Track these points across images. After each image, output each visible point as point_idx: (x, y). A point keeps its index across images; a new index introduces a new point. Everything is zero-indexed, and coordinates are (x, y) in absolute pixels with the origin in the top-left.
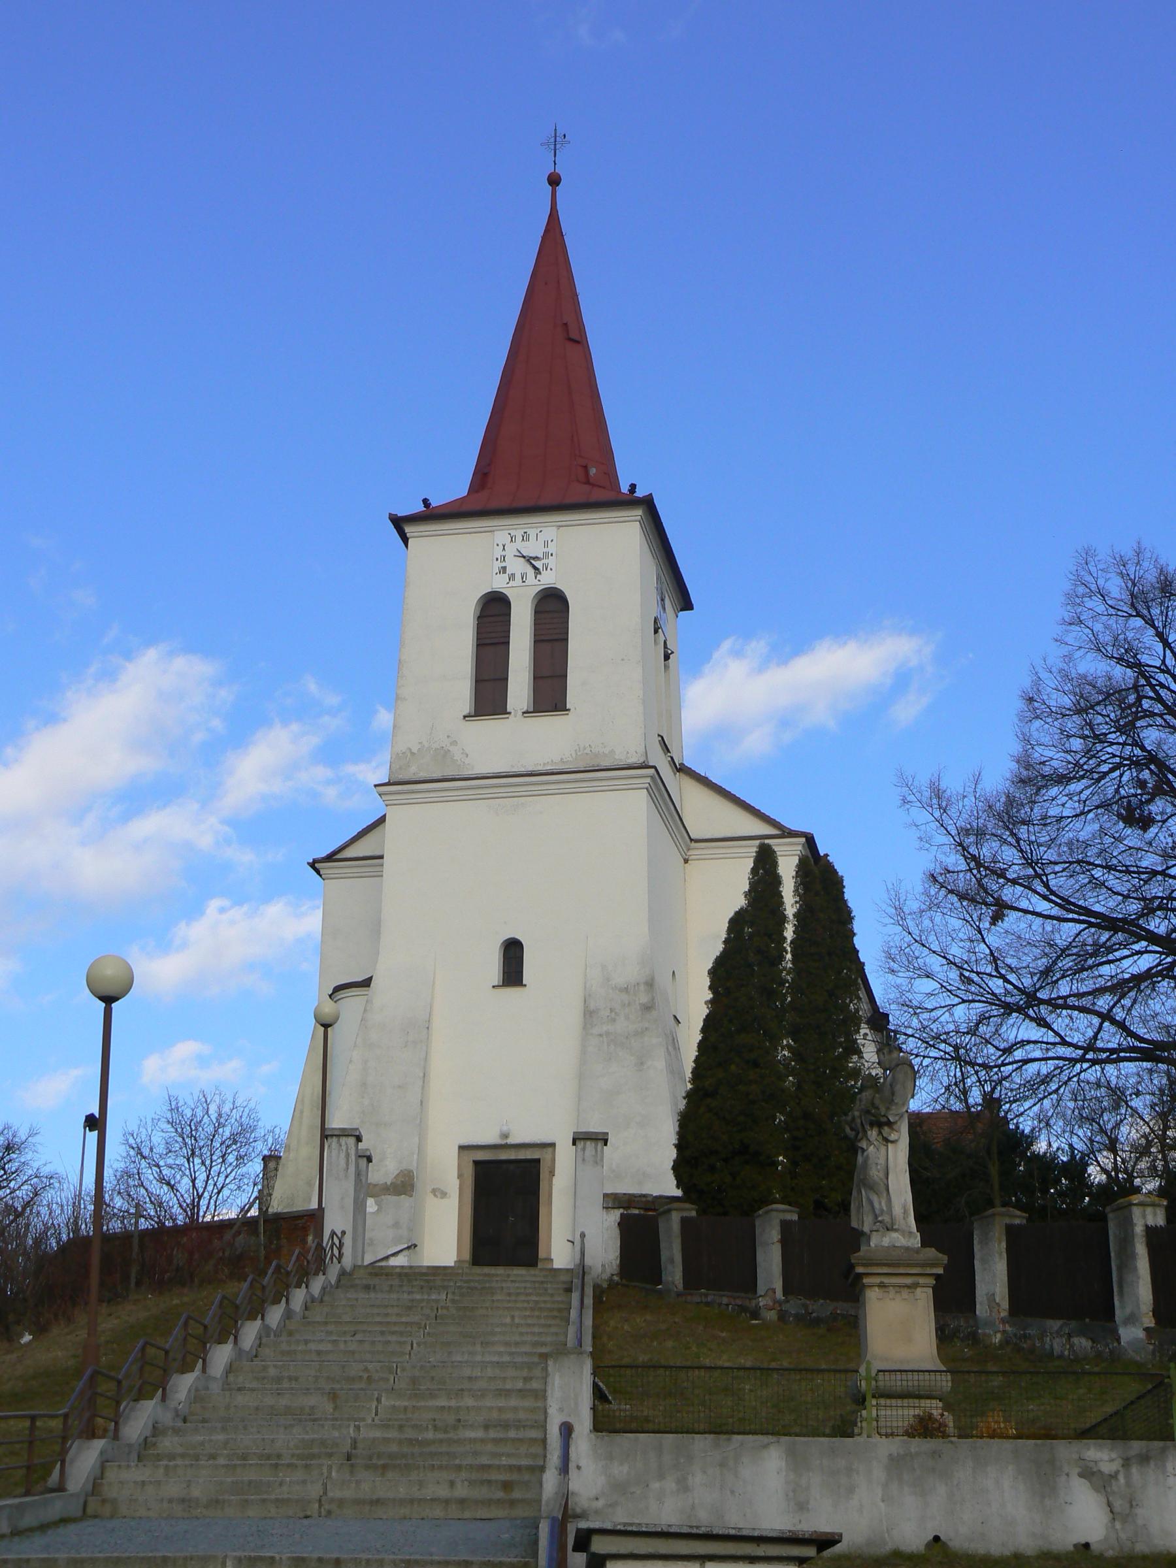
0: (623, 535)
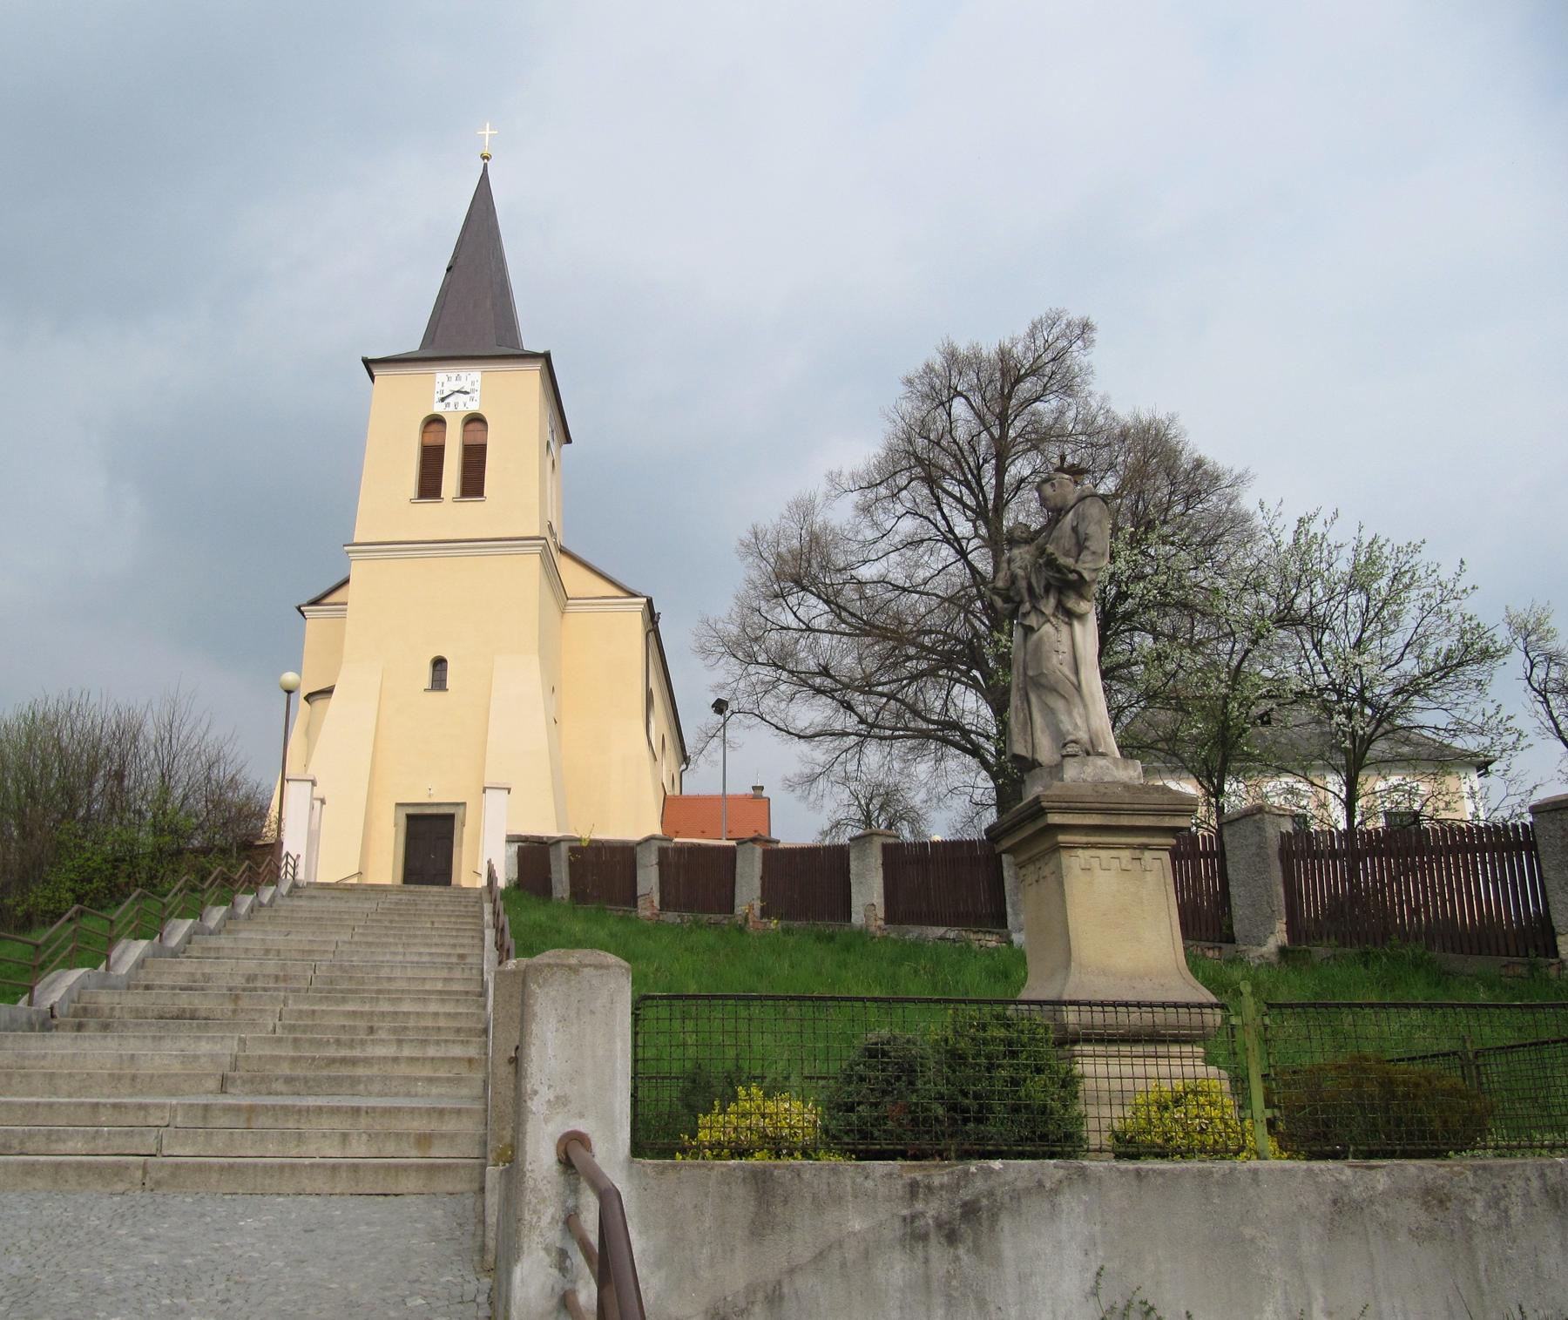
0: (529, 377)
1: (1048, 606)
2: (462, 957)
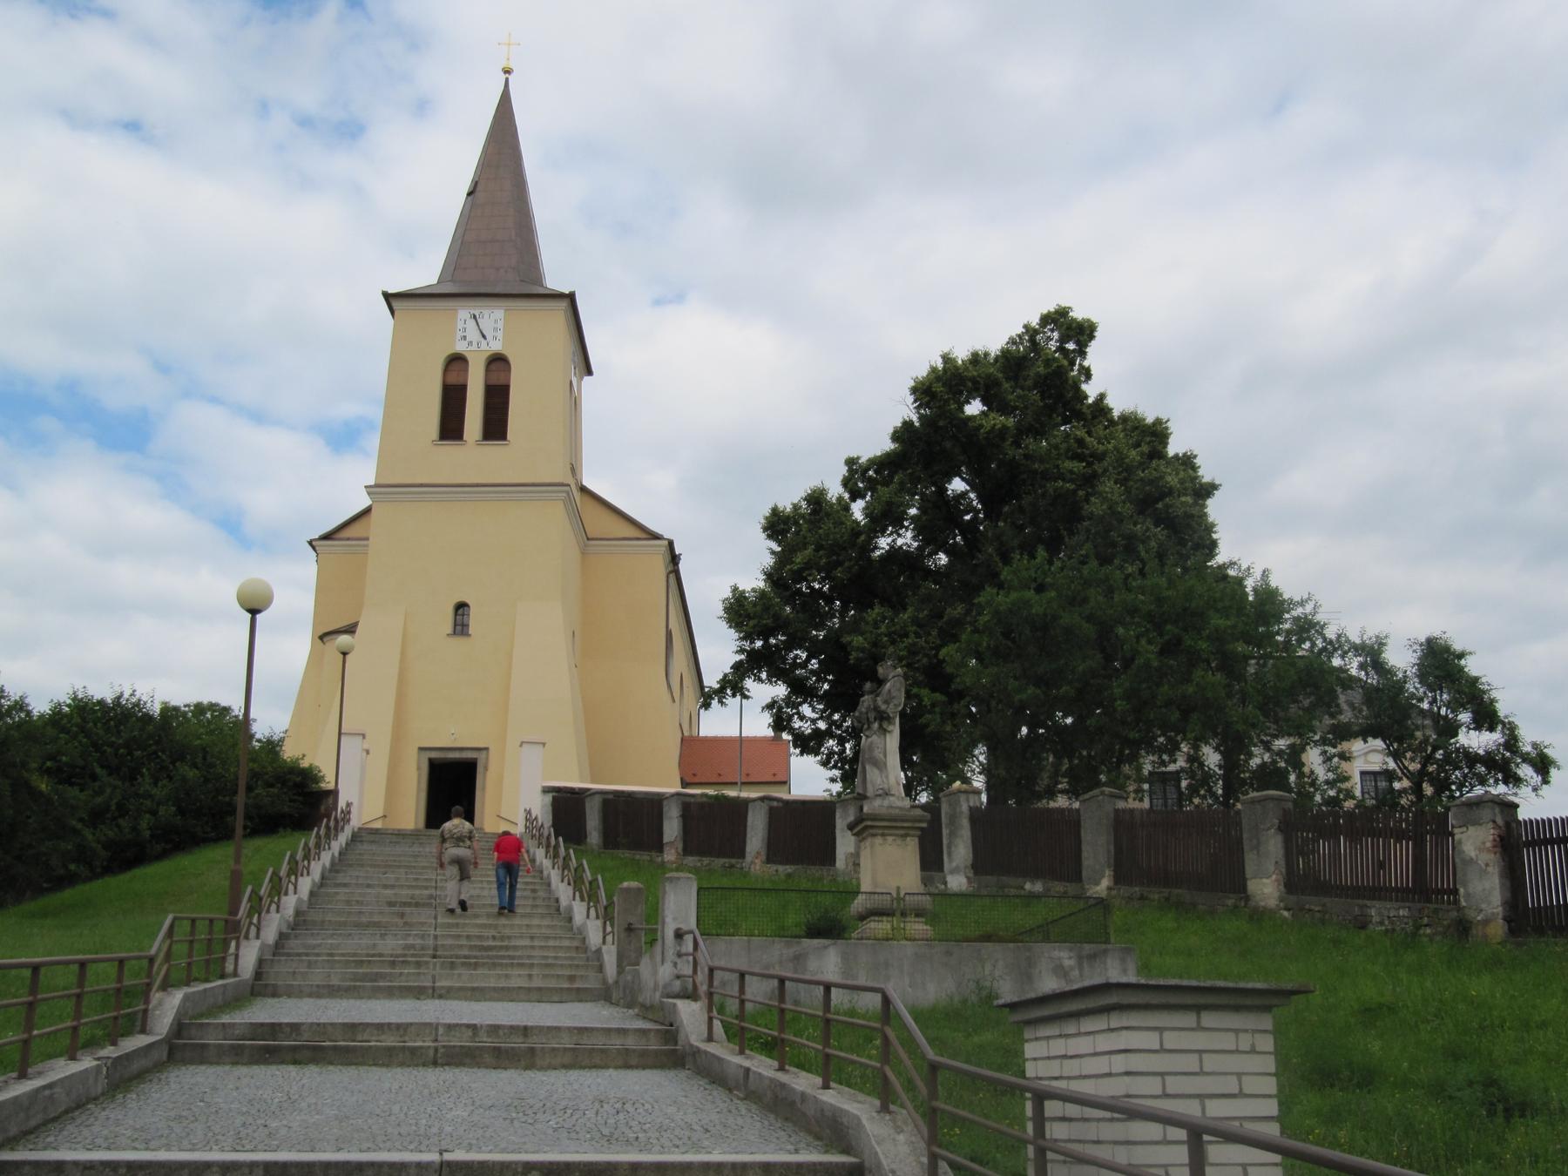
1: (876, 725)
2: (534, 891)
